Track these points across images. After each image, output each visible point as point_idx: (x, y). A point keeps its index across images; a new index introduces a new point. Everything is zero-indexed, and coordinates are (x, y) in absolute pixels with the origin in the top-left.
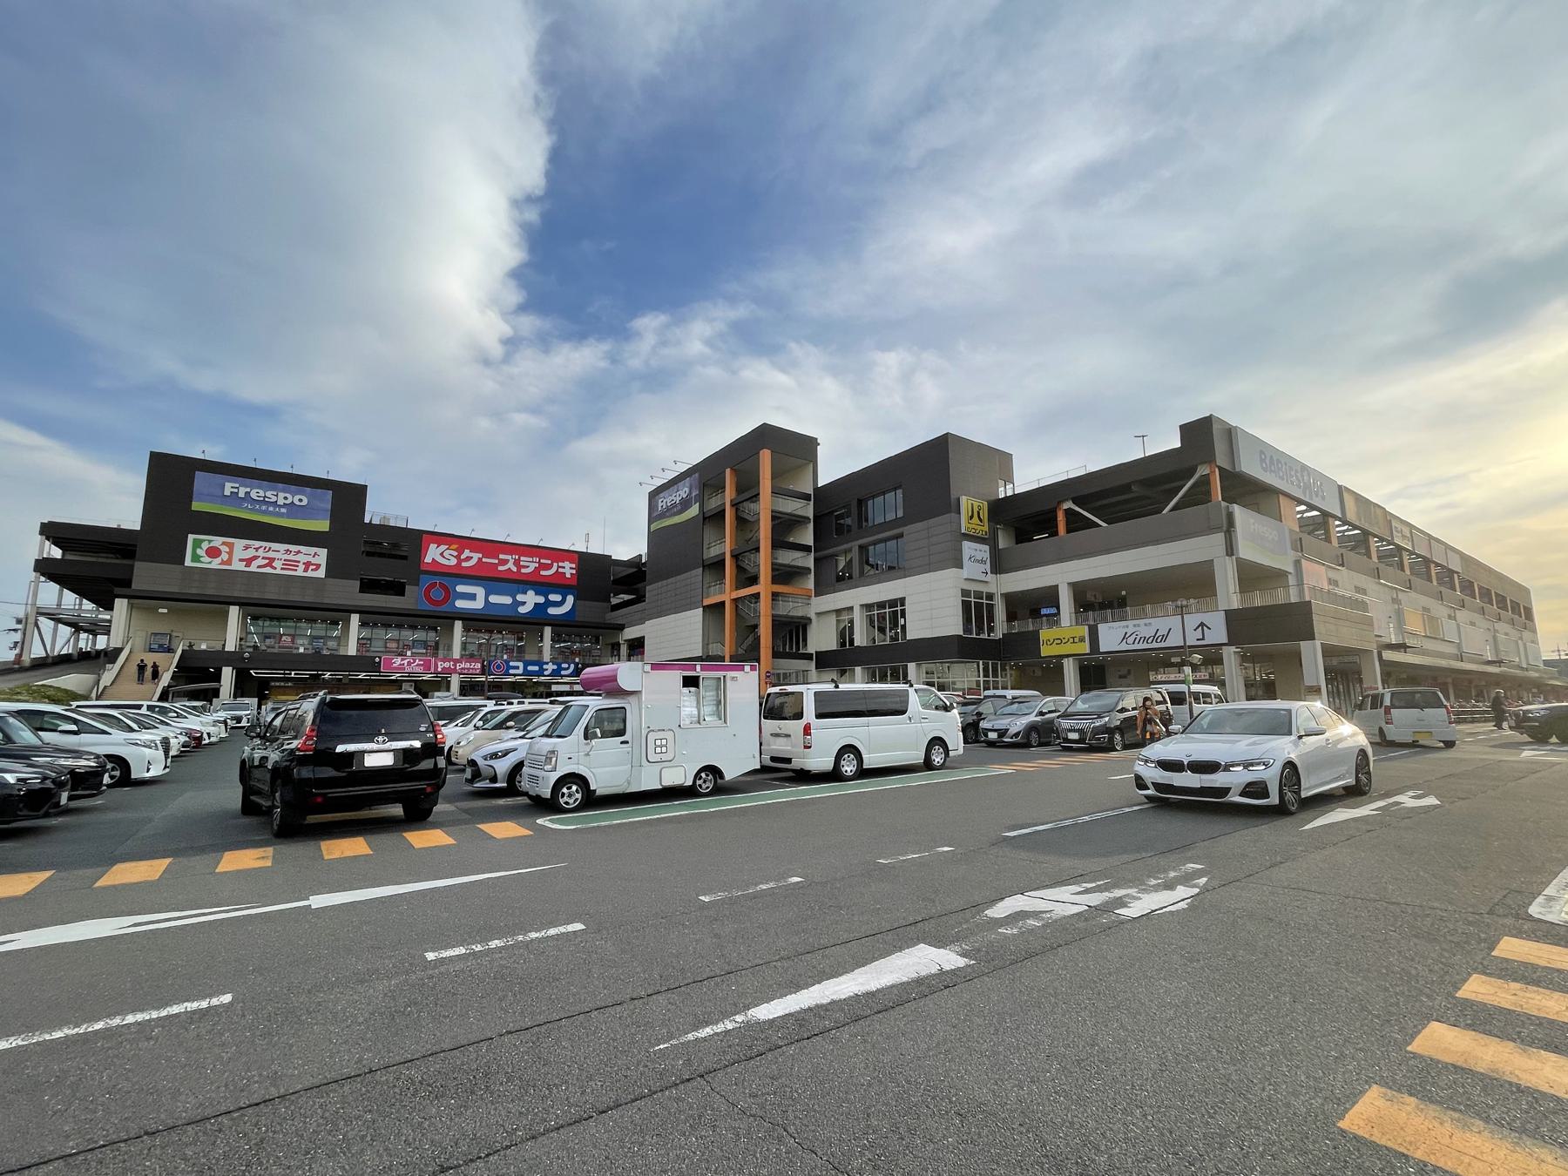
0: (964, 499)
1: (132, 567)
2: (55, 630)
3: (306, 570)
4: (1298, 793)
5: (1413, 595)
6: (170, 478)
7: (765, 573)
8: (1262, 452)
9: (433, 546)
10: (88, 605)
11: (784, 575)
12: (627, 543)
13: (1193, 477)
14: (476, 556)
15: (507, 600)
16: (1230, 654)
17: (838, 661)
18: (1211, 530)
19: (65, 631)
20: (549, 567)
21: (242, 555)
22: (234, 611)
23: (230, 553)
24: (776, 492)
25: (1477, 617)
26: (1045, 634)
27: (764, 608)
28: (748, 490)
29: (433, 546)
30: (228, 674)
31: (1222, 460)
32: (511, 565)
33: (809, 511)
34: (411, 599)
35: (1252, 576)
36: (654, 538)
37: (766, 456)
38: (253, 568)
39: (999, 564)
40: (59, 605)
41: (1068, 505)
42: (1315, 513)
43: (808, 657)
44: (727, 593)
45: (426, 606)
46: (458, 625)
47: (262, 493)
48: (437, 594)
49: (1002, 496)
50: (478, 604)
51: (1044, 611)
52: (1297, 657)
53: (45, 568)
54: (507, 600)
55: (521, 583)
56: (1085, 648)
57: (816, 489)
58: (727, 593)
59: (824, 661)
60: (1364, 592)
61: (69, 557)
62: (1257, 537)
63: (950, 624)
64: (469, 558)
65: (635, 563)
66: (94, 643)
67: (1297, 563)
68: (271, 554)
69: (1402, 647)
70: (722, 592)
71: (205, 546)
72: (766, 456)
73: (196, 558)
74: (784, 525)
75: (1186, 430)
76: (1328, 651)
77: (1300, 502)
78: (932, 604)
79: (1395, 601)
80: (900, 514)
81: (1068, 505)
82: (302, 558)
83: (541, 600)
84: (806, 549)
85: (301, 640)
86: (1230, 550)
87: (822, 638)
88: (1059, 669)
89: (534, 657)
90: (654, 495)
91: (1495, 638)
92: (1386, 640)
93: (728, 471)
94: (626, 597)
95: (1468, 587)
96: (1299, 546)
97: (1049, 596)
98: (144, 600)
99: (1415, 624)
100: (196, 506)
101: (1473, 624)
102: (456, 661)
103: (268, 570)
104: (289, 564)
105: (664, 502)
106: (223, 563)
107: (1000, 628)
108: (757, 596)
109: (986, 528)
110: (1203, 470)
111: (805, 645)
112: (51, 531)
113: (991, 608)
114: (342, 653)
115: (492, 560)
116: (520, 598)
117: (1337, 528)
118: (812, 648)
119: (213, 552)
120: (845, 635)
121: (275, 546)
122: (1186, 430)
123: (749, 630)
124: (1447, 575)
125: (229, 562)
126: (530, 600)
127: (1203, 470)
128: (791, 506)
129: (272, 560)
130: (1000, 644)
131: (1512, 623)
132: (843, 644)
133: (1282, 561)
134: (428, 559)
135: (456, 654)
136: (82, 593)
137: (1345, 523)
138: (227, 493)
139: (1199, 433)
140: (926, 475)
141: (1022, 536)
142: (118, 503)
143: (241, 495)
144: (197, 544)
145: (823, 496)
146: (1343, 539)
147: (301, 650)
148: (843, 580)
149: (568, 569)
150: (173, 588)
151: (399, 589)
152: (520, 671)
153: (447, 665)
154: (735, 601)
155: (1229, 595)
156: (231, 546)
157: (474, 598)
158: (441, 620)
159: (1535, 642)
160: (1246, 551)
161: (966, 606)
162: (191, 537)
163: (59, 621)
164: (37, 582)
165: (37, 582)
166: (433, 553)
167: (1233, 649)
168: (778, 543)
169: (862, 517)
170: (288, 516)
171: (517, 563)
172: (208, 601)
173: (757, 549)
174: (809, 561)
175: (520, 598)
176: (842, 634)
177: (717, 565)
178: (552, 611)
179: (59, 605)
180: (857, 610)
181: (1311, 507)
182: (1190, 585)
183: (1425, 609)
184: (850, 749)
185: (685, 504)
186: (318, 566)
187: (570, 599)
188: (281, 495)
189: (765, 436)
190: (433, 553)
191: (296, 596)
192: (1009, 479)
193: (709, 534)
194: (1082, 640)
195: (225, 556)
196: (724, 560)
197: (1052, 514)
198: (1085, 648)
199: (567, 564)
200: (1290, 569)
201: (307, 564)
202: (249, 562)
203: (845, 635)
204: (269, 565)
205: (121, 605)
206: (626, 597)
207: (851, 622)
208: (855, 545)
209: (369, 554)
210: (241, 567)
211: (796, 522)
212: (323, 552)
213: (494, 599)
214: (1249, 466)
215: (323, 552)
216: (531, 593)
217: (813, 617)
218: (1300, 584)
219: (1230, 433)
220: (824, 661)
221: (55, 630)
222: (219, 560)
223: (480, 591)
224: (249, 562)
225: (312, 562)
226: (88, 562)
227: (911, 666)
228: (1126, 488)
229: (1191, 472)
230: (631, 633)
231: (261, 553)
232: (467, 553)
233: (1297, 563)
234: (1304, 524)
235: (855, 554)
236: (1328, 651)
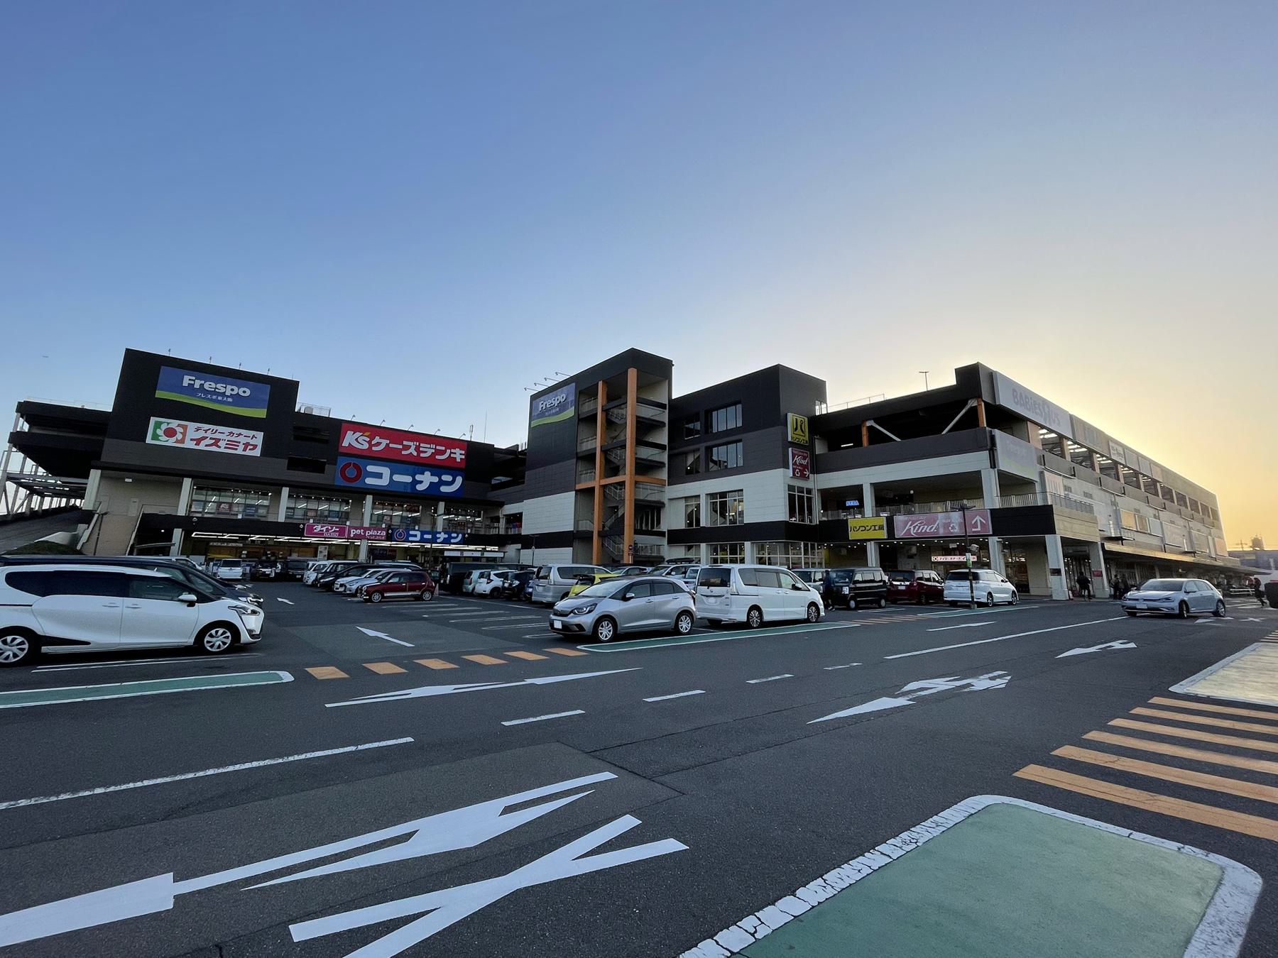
0: (790, 416)
1: (101, 444)
2: (17, 491)
3: (245, 450)
5: (1126, 498)
6: (142, 371)
8: (1014, 391)
9: (349, 433)
10: (41, 471)
11: (644, 468)
12: (509, 431)
13: (967, 409)
15: (408, 479)
16: (994, 542)
17: (688, 536)
19: (23, 492)
20: (443, 453)
21: (192, 436)
22: (187, 482)
23: (184, 434)
24: (640, 401)
25: (1176, 517)
29: (349, 433)
30: (178, 534)
31: (986, 397)
32: (412, 450)
33: (665, 417)
34: (331, 475)
35: (1010, 483)
36: (532, 430)
37: (632, 374)
38: (202, 447)
40: (22, 470)
41: (869, 423)
42: (1053, 435)
43: (662, 534)
44: (596, 480)
45: (340, 482)
46: (369, 498)
47: (213, 385)
48: (351, 472)
49: (818, 413)
50: (384, 482)
51: (849, 503)
52: (1043, 547)
53: (18, 440)
54: (408, 479)
55: (419, 465)
56: (883, 534)
57: (670, 400)
58: (596, 480)
59: (675, 537)
60: (1091, 496)
61: (35, 431)
62: (1014, 455)
63: (777, 512)
64: (378, 444)
65: (513, 451)
66: (41, 503)
67: (1041, 474)
68: (217, 436)
69: (1119, 539)
71: (164, 427)
72: (632, 374)
73: (155, 437)
75: (961, 373)
76: (1066, 542)
77: (1043, 427)
78: (764, 495)
79: (1114, 504)
80: (740, 424)
82: (242, 440)
83: (436, 479)
85: (238, 504)
86: (993, 464)
87: (674, 519)
88: (863, 550)
89: (428, 528)
90: (534, 398)
91: (1190, 533)
92: (1107, 534)
93: (600, 383)
94: (503, 479)
95: (1168, 493)
96: (1042, 461)
97: (856, 492)
98: (114, 472)
99: (1128, 521)
100: (160, 394)
101: (1172, 522)
102: (366, 529)
103: (214, 449)
105: (541, 404)
106: (177, 441)
107: (818, 515)
108: (622, 484)
111: (659, 523)
112: (26, 410)
113: (809, 500)
114: (271, 519)
115: (398, 446)
116: (418, 477)
117: (1070, 447)
118: (664, 527)
119: (170, 433)
120: (693, 517)
121: (221, 429)
122: (961, 373)
123: (612, 510)
124: (1152, 485)
125: (182, 441)
126: (426, 479)
127: (972, 403)
128: (649, 412)
129: (218, 440)
130: (814, 532)
131: (1202, 521)
132: (690, 524)
133: (1029, 473)
134: (345, 444)
135: (366, 524)
136: (39, 462)
137: (1075, 443)
138: (185, 383)
139: (970, 377)
140: (765, 397)
141: (833, 446)
142: (97, 392)
143: (197, 386)
144: (158, 425)
146: (1074, 456)
147: (240, 517)
148: (693, 474)
149: (459, 455)
150: (135, 461)
151: (319, 468)
152: (418, 538)
153: (358, 532)
154: (604, 487)
155: (992, 498)
156: (185, 428)
157: (381, 476)
158: (358, 495)
159: (1221, 537)
161: (791, 498)
162: (153, 420)
163: (20, 485)
164: (10, 452)
165: (10, 452)
166: (350, 439)
167: (996, 539)
168: (640, 442)
169: (708, 425)
171: (417, 449)
172: (166, 471)
173: (624, 447)
174: (664, 458)
175: (418, 477)
176: (689, 516)
177: (589, 458)
178: (444, 489)
179: (22, 470)
181: (1051, 431)
182: (961, 489)
183: (1137, 511)
184: (755, 608)
185: (562, 407)
186: (255, 447)
187: (459, 480)
188: (229, 387)
189: (634, 358)
190: (350, 439)
191: (236, 472)
192: (823, 399)
193: (584, 431)
194: (881, 528)
195: (179, 436)
196: (595, 454)
197: (858, 429)
198: (883, 534)
199: (457, 451)
200: (1036, 478)
201: (247, 445)
202: (198, 441)
203: (693, 517)
205: (95, 475)
206: (503, 479)
207: (698, 507)
208: (702, 446)
209: (296, 438)
210: (192, 445)
211: (656, 425)
212: (260, 435)
213: (397, 478)
214: (1005, 400)
215: (260, 435)
216: (428, 474)
217: (666, 502)
218: (1044, 492)
219: (992, 375)
220: (675, 537)
221: (17, 491)
222: (174, 439)
223: (386, 471)
224: (198, 441)
225: (250, 443)
226: (57, 437)
227: (747, 545)
230: (510, 509)
231: (209, 434)
232: (377, 439)
233: (1041, 474)
234: (1045, 443)
235: (702, 452)
236: (1066, 542)
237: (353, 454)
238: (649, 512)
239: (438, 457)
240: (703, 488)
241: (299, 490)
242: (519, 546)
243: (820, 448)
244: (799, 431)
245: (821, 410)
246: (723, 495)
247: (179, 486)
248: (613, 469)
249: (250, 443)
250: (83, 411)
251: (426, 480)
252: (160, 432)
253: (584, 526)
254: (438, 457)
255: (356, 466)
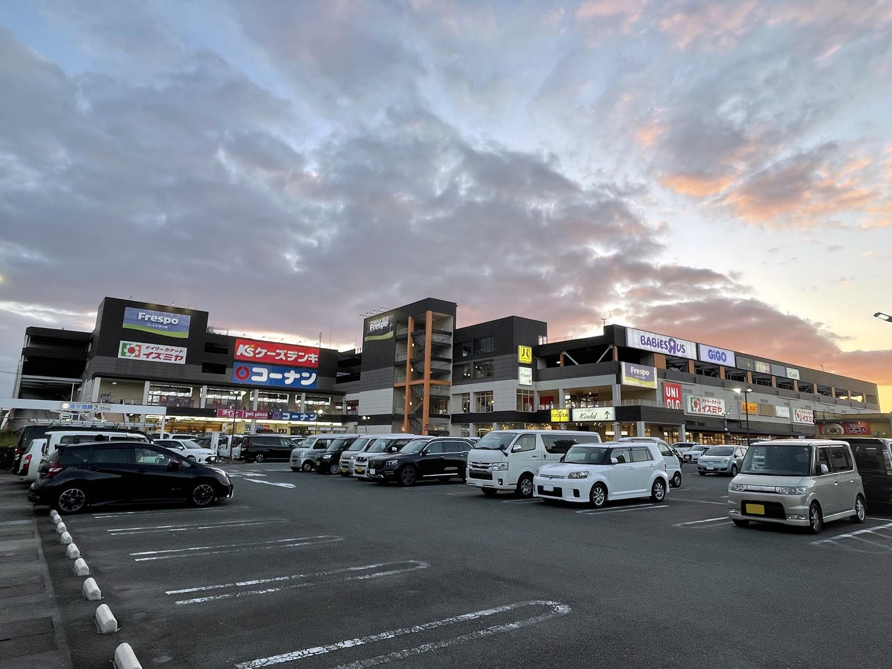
4: (820, 517)
6: (113, 310)
7: (427, 373)
11: (437, 375)
12: (349, 344)
14: (264, 351)
15: (279, 376)
18: (611, 373)
20: (302, 357)
21: (144, 352)
23: (140, 351)
26: (554, 412)
27: (426, 391)
28: (420, 326)
29: (241, 346)
32: (282, 356)
34: (229, 376)
36: (365, 344)
38: (150, 359)
39: (536, 377)
49: (541, 343)
50: (264, 379)
54: (279, 376)
55: (283, 367)
57: (455, 330)
59: (457, 419)
64: (260, 353)
70: (405, 381)
71: (128, 347)
72: (429, 316)
74: (438, 348)
81: (565, 353)
83: (298, 376)
84: (449, 361)
86: (619, 380)
87: (455, 407)
102: (255, 412)
103: (157, 360)
104: (168, 357)
105: (374, 326)
109: (530, 360)
110: (611, 347)
115: (274, 357)
119: (132, 350)
121: (161, 346)
125: (138, 356)
128: (439, 338)
129: (159, 354)
134: (238, 353)
144: (124, 346)
145: (458, 333)
149: (314, 358)
154: (412, 386)
156: (140, 347)
157: (262, 376)
160: (626, 381)
162: (122, 342)
170: (169, 330)
171: (286, 355)
174: (450, 367)
175: (286, 375)
177: (402, 366)
178: (304, 383)
180: (472, 395)
185: (385, 330)
186: (182, 357)
187: (314, 376)
188: (166, 319)
189: (429, 304)
190: (242, 350)
191: (169, 376)
192: (544, 334)
193: (398, 347)
195: (137, 353)
201: (177, 357)
202: (148, 355)
204: (158, 357)
212: (185, 350)
215: (185, 350)
216: (293, 372)
220: (457, 419)
223: (265, 371)
224: (148, 355)
225: (178, 355)
228: (585, 349)
229: (606, 346)
230: (350, 397)
231: (154, 351)
232: (259, 349)
237: (244, 360)
238: (437, 402)
239: (300, 360)
240: (472, 388)
241: (213, 386)
242: (356, 423)
243: (540, 366)
244: (525, 356)
245: (541, 341)
246: (483, 393)
247: (144, 385)
248: (419, 375)
249: (178, 355)
250: (63, 331)
251: (291, 377)
252: (126, 350)
253: (399, 411)
254: (300, 360)
255: (245, 368)
